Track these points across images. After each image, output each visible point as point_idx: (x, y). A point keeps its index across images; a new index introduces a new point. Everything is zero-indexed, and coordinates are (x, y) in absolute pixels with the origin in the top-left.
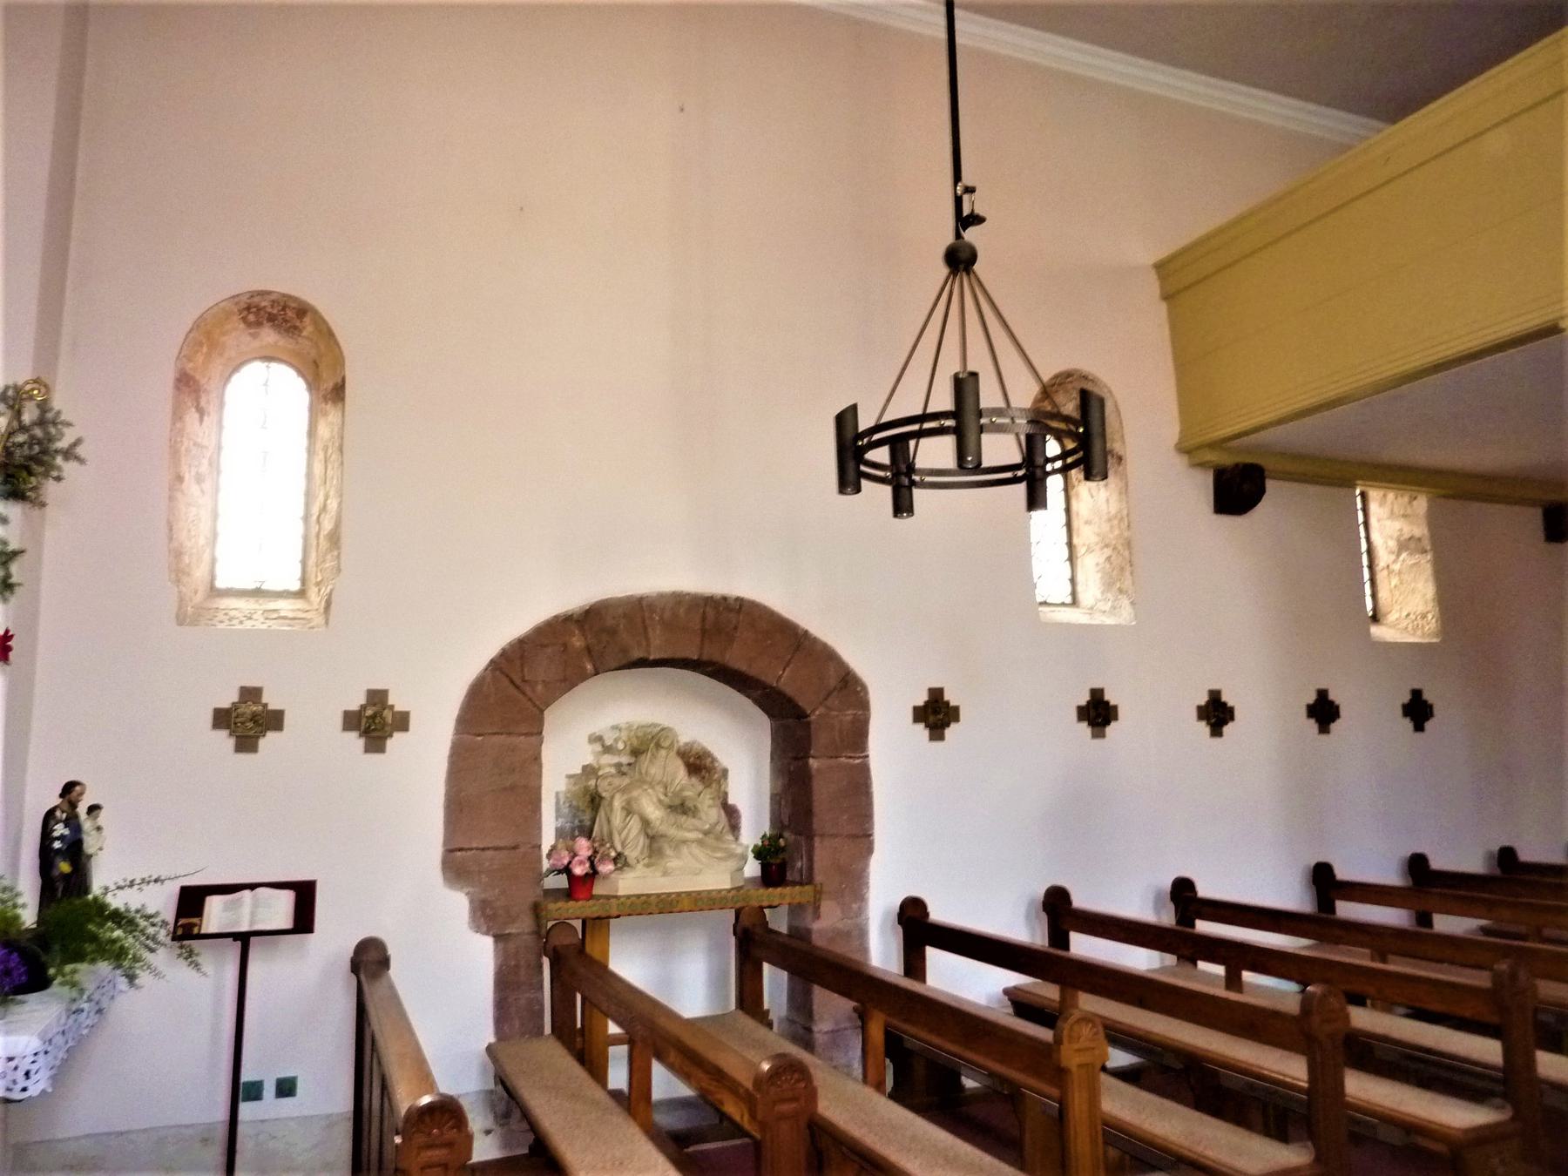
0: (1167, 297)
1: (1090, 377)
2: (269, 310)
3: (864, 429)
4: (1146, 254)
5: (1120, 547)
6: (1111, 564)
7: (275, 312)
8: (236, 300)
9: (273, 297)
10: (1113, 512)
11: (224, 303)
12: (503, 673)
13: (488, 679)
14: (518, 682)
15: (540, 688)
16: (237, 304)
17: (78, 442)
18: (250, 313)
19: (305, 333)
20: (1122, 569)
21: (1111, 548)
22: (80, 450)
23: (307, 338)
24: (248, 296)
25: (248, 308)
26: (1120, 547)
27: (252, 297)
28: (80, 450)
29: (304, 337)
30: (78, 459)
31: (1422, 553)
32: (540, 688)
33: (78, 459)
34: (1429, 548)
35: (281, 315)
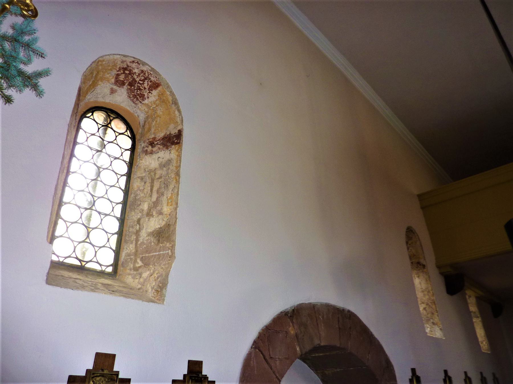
0: (423, 208)
1: (413, 231)
2: (135, 77)
3: (115, 248)
4: (416, 192)
5: (430, 304)
6: (426, 311)
7: (138, 80)
8: (124, 59)
9: (145, 68)
10: (424, 288)
11: (118, 56)
12: (260, 350)
13: (253, 356)
14: (267, 357)
15: (278, 363)
16: (123, 62)
17: (39, 75)
18: (124, 73)
19: (146, 101)
20: (433, 314)
21: (425, 304)
22: (42, 82)
23: (147, 105)
24: (133, 59)
25: (125, 69)
26: (430, 304)
27: (133, 62)
28: (42, 82)
29: (145, 104)
30: (35, 87)
31: (477, 318)
32: (278, 363)
33: (35, 87)
34: (479, 316)
35: (139, 83)
